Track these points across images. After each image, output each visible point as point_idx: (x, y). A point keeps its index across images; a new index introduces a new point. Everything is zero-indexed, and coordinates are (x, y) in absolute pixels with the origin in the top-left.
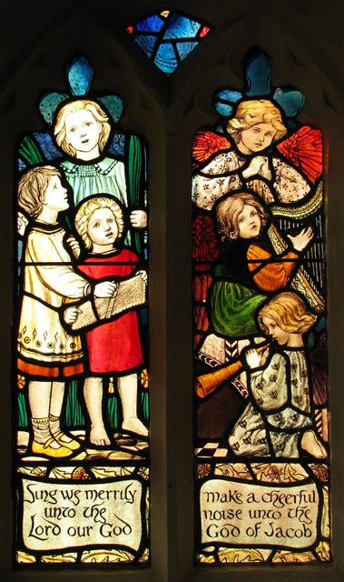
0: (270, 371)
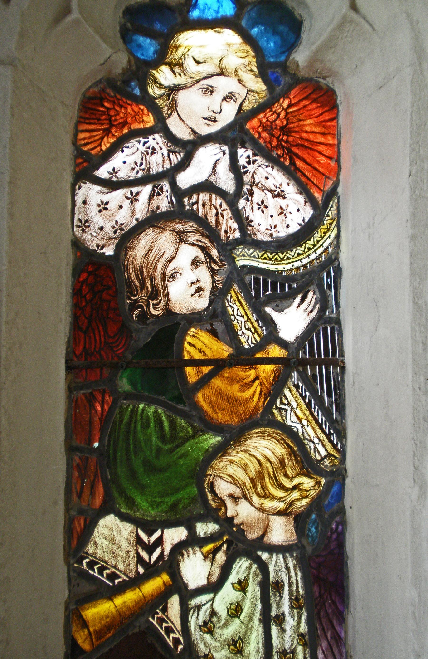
0: (228, 594)
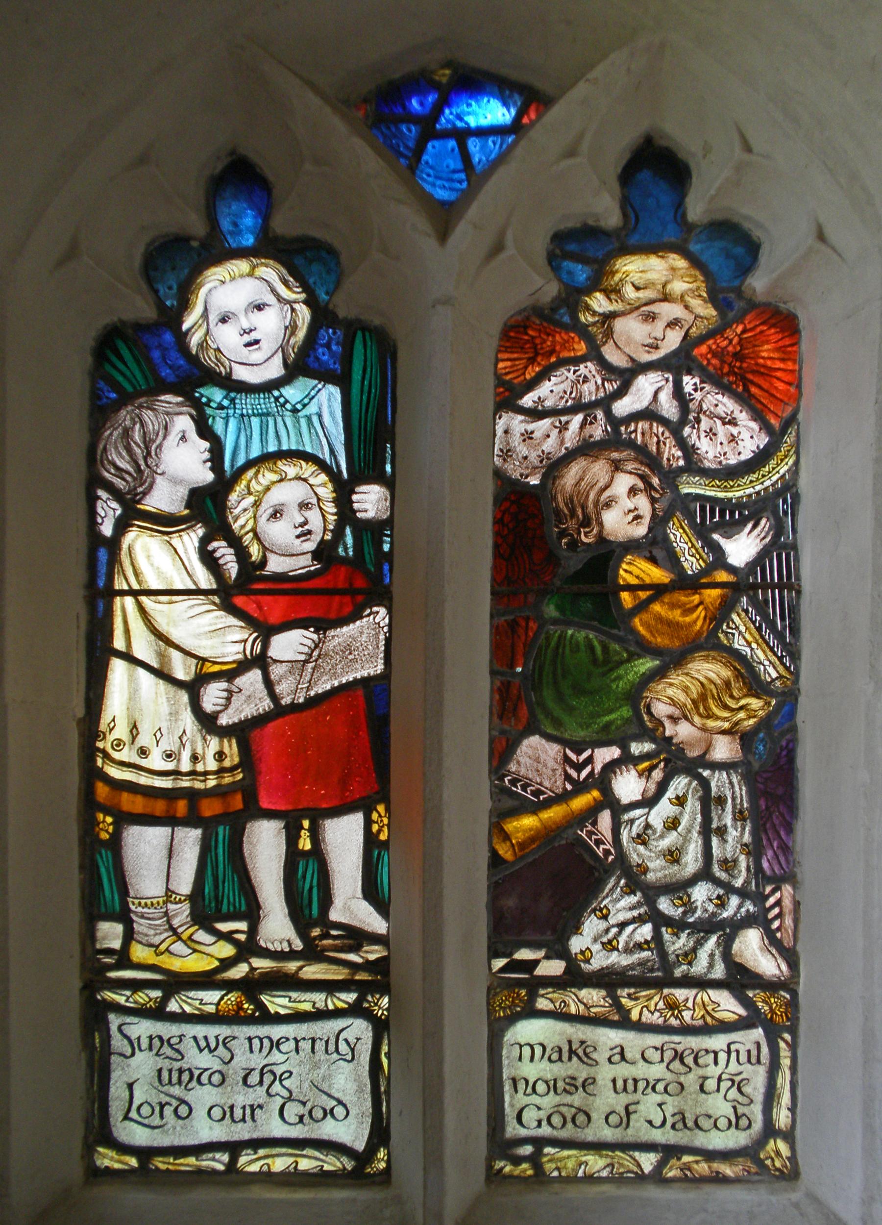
0: (664, 809)
